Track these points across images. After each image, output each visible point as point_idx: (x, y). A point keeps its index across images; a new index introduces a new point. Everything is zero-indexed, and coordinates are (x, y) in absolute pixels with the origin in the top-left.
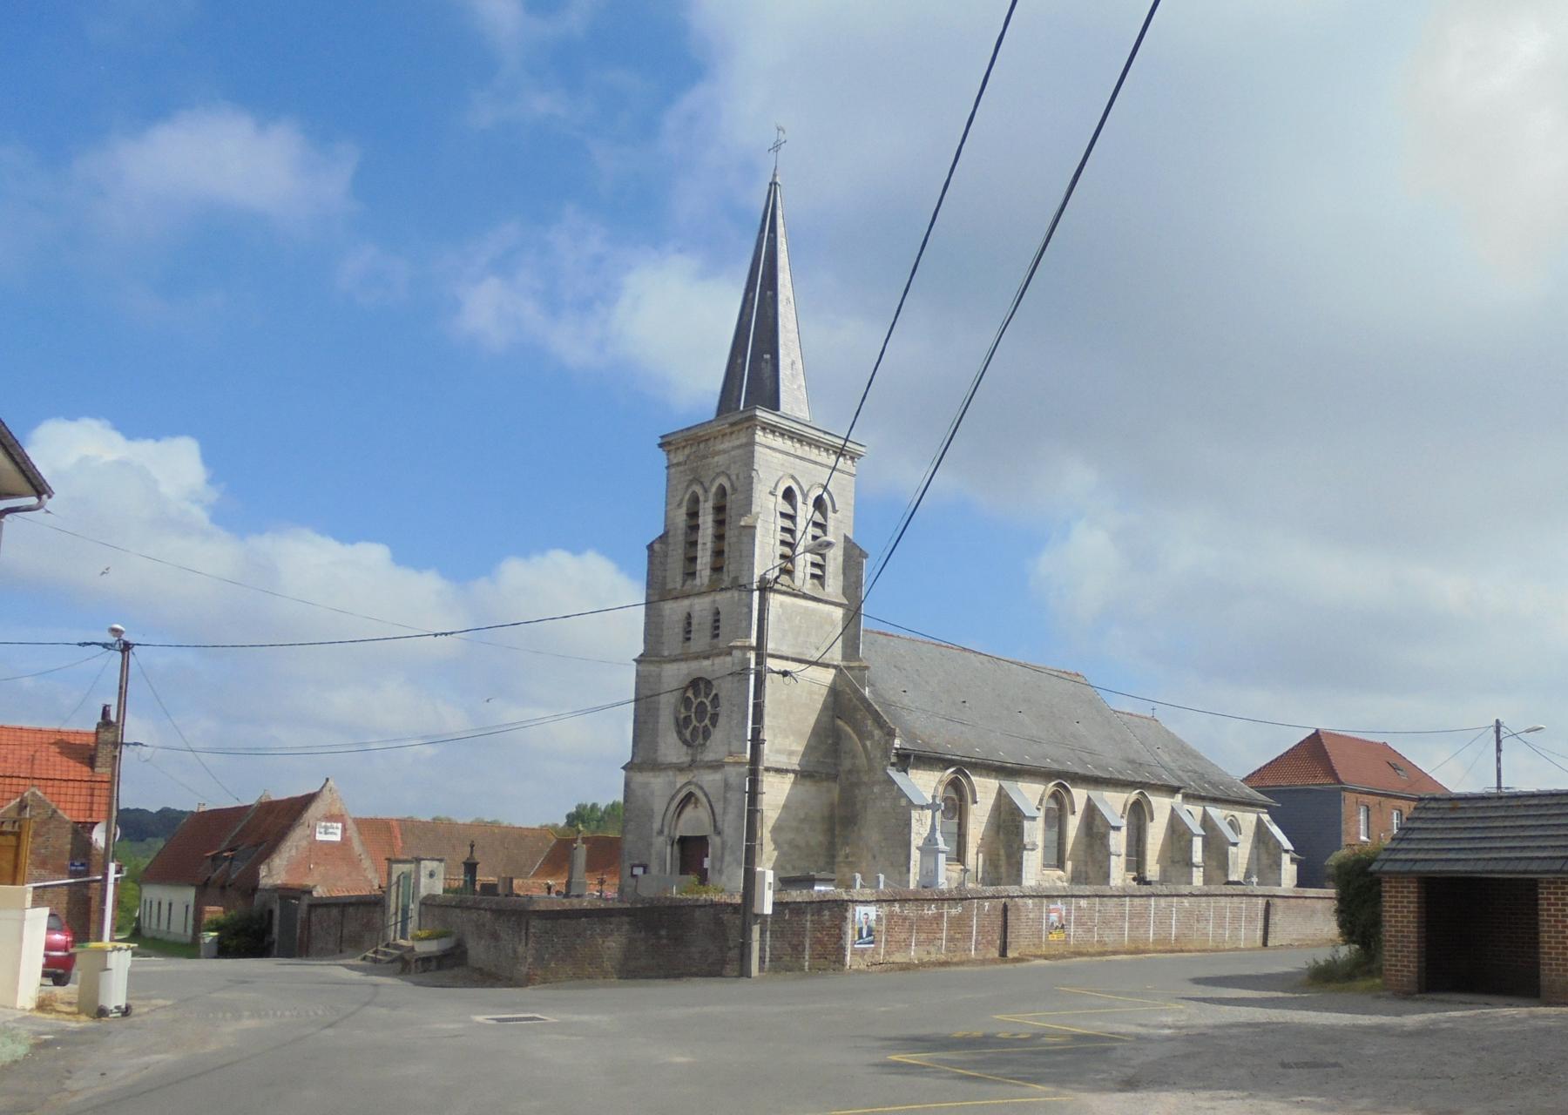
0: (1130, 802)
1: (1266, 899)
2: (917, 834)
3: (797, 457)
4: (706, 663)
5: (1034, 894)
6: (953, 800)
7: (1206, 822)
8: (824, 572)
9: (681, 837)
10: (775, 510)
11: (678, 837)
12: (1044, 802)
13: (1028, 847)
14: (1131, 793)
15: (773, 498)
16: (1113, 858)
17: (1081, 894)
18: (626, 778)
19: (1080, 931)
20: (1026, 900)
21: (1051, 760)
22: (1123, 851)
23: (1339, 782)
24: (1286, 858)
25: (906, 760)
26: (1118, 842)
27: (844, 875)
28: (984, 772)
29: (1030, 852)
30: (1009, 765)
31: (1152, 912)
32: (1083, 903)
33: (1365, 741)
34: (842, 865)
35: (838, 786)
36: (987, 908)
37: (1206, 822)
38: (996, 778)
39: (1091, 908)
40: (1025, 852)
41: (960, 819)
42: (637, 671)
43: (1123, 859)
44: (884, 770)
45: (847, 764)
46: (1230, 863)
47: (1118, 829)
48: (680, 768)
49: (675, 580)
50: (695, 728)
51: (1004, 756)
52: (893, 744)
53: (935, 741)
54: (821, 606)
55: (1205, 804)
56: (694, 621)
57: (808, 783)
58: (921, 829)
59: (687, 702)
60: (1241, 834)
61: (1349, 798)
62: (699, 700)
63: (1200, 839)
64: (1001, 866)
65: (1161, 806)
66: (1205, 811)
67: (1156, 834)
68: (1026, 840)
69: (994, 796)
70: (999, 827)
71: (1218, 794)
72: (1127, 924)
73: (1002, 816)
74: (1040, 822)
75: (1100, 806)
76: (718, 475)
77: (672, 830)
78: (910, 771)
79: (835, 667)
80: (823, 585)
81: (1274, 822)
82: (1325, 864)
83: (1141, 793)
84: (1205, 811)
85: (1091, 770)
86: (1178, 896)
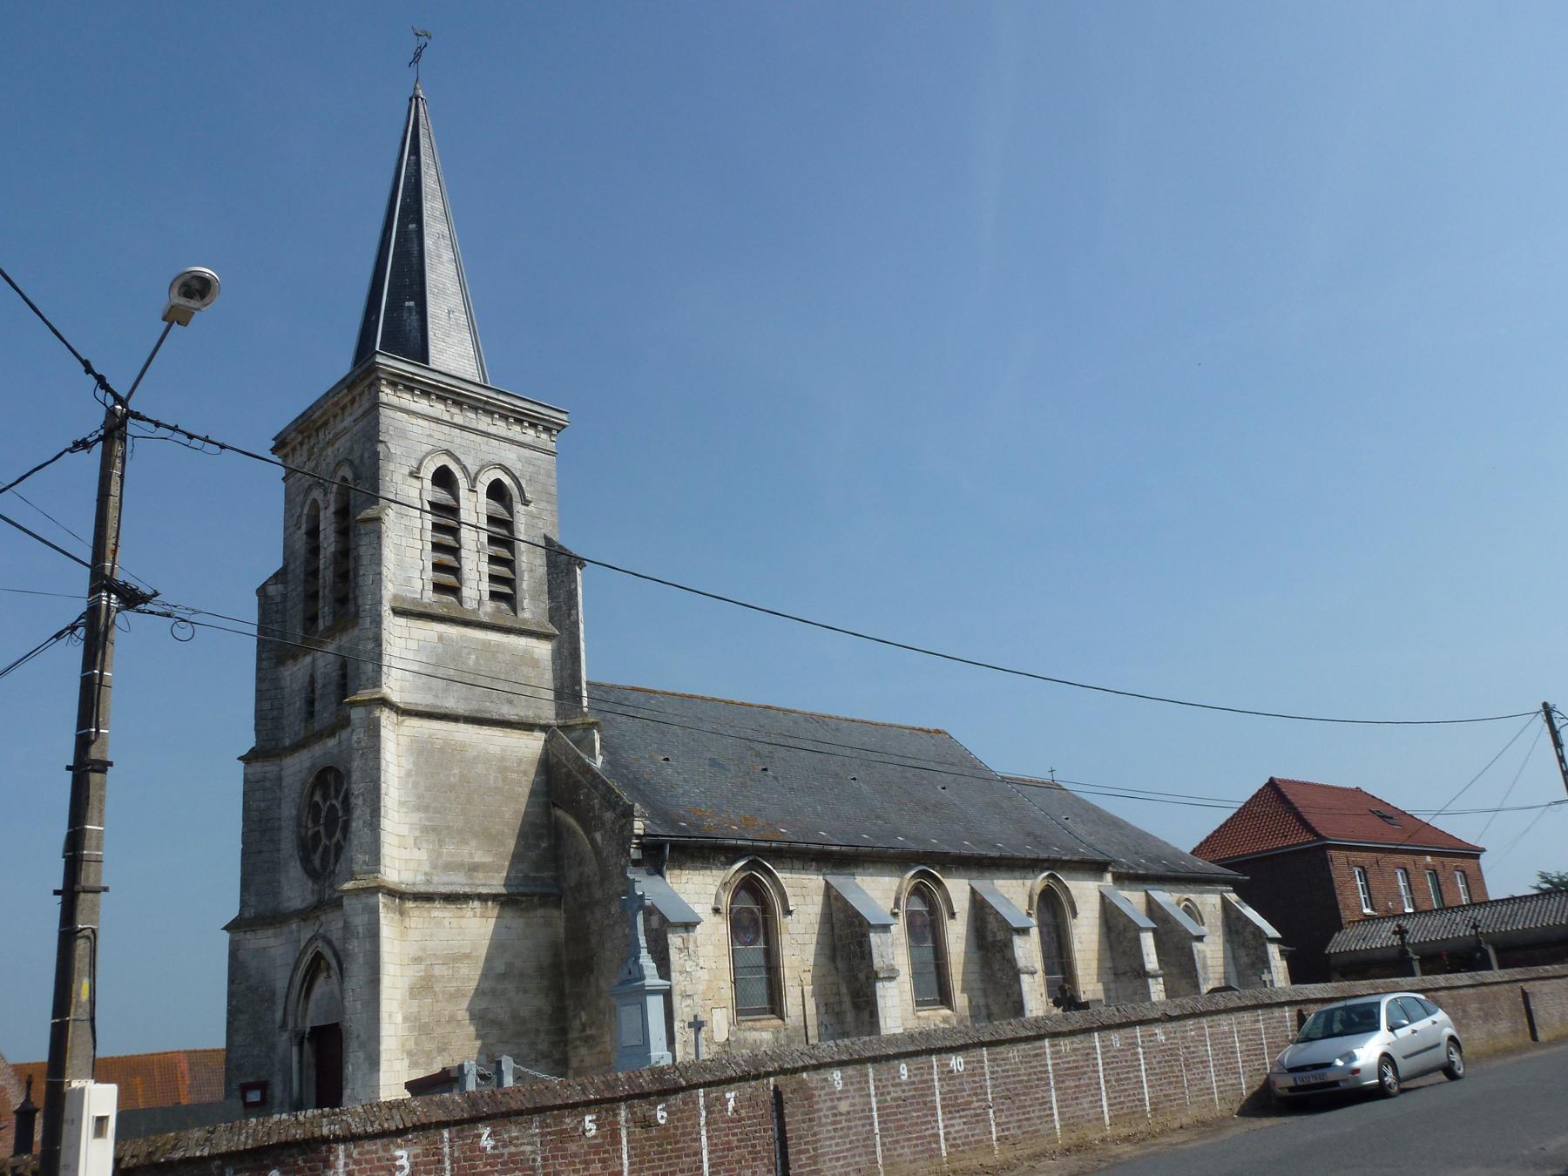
0: (1038, 890)
1: (1295, 1009)
2: (681, 973)
3: (455, 426)
4: (332, 742)
5: (845, 1057)
6: (751, 912)
7: (1153, 909)
8: (514, 589)
9: (313, 1028)
10: (421, 499)
11: (308, 1030)
12: (903, 903)
13: (881, 976)
14: (1036, 877)
15: (417, 483)
16: (1025, 978)
17: (948, 1044)
18: (232, 942)
19: (958, 1123)
20: (824, 1073)
21: (906, 838)
22: (1039, 965)
23: (1320, 837)
24: (1273, 951)
25: (657, 856)
26: (1028, 951)
27: (582, 1061)
28: (797, 864)
29: (887, 984)
30: (834, 848)
31: (1100, 1062)
32: (957, 1062)
33: (1333, 788)
34: (578, 1043)
35: (563, 915)
36: (731, 1104)
37: (1153, 909)
38: (819, 871)
39: (974, 1071)
40: (879, 985)
41: (767, 942)
42: (245, 774)
43: (1040, 977)
44: (623, 874)
45: (572, 877)
46: (1199, 966)
47: (1024, 931)
48: (304, 915)
49: (296, 632)
50: (326, 848)
51: (827, 836)
52: (632, 828)
53: (710, 822)
54: (512, 640)
55: (1146, 887)
56: (319, 684)
57: (509, 914)
58: (689, 963)
59: (314, 809)
60: (1203, 924)
61: (1338, 859)
62: (328, 803)
63: (1150, 934)
64: (845, 1012)
65: (1086, 893)
66: (1148, 895)
67: (1085, 934)
68: (877, 963)
69: (819, 900)
70: (834, 949)
71: (1160, 870)
72: (1053, 1093)
73: (837, 931)
74: (899, 928)
75: (989, 899)
76: (338, 464)
77: (300, 1020)
78: (668, 874)
79: (544, 728)
80: (515, 610)
81: (1245, 902)
82: (1332, 948)
83: (1051, 876)
84: (1148, 895)
85: (968, 847)
86: (1141, 1023)
